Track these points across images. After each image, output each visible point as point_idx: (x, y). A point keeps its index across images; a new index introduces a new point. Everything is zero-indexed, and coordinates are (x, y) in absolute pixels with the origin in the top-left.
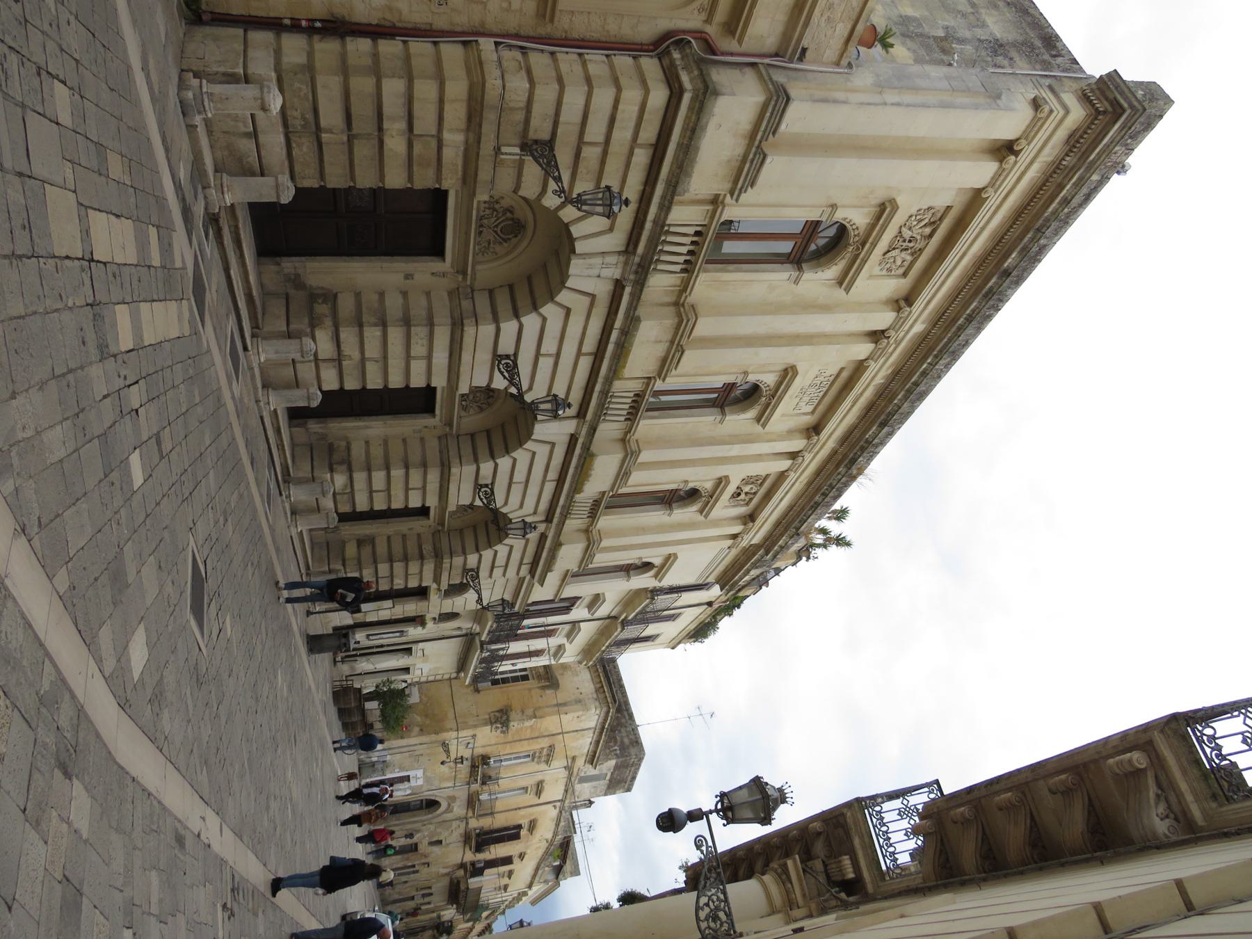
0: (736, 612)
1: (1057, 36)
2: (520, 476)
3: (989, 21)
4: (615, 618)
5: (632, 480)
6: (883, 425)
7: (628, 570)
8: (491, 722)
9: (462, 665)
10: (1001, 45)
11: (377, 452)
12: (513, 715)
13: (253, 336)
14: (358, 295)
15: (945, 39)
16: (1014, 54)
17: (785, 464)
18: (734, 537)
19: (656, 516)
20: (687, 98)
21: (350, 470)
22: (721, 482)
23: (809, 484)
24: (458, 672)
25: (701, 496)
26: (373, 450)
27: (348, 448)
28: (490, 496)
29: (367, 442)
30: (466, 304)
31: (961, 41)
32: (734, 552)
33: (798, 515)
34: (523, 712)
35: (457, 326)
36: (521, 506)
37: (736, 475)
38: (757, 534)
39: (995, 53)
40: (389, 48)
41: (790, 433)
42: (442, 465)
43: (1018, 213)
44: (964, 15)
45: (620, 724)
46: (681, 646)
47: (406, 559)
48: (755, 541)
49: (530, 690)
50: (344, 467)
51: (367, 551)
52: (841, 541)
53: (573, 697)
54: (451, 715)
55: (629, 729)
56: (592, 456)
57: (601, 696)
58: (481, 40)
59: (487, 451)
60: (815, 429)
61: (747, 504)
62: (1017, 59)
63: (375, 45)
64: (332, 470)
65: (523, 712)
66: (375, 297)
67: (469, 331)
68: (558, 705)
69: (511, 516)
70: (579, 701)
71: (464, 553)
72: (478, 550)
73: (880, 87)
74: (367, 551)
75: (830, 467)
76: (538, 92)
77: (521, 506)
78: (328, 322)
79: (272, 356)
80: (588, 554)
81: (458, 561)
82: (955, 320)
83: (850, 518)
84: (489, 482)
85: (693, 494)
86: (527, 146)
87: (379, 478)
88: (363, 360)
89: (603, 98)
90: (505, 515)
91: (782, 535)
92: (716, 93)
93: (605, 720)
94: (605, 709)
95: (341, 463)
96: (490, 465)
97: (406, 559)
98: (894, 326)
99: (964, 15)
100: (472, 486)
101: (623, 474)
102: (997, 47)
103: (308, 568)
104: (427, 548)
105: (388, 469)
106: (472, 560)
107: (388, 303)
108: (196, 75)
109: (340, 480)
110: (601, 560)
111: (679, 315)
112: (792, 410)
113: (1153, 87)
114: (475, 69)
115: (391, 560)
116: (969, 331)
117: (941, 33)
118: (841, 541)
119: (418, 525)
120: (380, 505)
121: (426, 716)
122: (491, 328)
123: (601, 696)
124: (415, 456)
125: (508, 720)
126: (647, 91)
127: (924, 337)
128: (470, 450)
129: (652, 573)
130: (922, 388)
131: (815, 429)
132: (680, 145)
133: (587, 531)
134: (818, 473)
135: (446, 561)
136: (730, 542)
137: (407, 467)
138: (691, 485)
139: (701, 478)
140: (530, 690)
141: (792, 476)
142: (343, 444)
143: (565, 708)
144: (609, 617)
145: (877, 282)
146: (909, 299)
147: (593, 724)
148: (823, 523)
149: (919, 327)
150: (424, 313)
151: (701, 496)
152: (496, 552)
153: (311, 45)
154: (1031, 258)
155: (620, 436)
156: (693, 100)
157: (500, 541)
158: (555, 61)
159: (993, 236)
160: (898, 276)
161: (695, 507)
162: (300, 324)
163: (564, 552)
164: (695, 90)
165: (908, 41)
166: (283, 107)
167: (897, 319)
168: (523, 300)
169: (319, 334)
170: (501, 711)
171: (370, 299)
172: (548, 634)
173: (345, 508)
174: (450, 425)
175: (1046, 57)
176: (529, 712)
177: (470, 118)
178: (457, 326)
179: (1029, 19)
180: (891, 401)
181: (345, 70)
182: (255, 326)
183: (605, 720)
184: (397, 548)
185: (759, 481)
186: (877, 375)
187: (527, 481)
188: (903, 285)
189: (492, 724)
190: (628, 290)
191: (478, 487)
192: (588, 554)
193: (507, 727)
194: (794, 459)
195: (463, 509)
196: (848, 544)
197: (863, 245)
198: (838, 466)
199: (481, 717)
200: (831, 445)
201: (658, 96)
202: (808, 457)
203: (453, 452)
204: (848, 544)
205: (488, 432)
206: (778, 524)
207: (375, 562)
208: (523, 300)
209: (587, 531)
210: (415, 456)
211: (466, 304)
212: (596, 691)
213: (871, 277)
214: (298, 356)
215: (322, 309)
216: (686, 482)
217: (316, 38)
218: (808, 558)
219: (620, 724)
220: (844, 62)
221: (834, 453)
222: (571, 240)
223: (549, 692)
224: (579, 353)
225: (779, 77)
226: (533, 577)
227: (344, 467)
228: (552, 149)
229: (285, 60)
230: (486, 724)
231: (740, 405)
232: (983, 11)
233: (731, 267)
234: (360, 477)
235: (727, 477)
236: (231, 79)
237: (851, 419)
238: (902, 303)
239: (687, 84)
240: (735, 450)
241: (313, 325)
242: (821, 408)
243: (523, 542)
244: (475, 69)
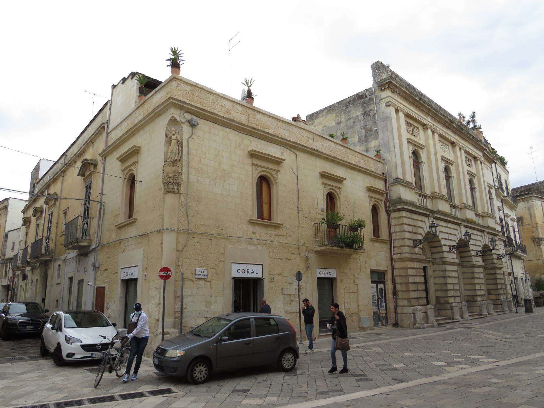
0: (385, 64)
1: (358, 94)
2: (446, 236)
3: (355, 115)
4: (502, 200)
5: (410, 180)
6: (453, 122)
7: (491, 199)
8: (539, 245)
9: (519, 258)
10: (365, 113)
11: (469, 287)
12: (536, 236)
13: (453, 319)
14: (436, 291)
15: (366, 130)
16: (368, 109)
17: (462, 151)
18: (481, 163)
19: (424, 168)
20: (405, 207)
21: (476, 295)
22: (409, 142)
23: (466, 141)
24: (521, 259)
25: (416, 150)
26: (468, 288)
27: (468, 296)
28: (419, 241)
29: (465, 290)
30: (438, 260)
31: (366, 125)
32: (486, 162)
33: (475, 142)
34: (534, 232)
35: (445, 263)
36: (455, 235)
37: (405, 135)
38: (479, 154)
39: (369, 115)
40: (398, 280)
41: (454, 152)
42: (472, 267)
43: (407, 100)
44: (354, 122)
45: (537, 189)
46: (507, 169)
47: (496, 279)
48: (481, 154)
49: (523, 229)
50: (475, 297)
51: (493, 292)
52: (473, 116)
53: (527, 211)
54: (536, 262)
55: (540, 185)
56: (467, 219)
57: (526, 199)
58: (393, 258)
59: (440, 248)
60: (453, 144)
61: (418, 128)
62: (370, 108)
63: (398, 283)
64: (476, 301)
65: (534, 232)
66: (437, 286)
67: (447, 260)
68: (531, 217)
69: (426, 232)
70: (529, 209)
71: (493, 259)
72: (441, 246)
73: (389, 152)
74: (493, 292)
75: (462, 135)
76: (407, 244)
77: (455, 235)
78: (447, 299)
79: (459, 315)
80: (442, 198)
81: (474, 259)
82: (429, 110)
83: (463, 113)
84: (448, 247)
85: (415, 154)
86: (415, 246)
87: (478, 287)
88: (454, 290)
89: (406, 228)
90: (426, 234)
91: (481, 146)
92: (400, 198)
93: (538, 197)
94: (533, 198)
95: (473, 298)
96: (444, 247)
97: (445, 277)
98: (402, 112)
99: (354, 122)
100: (450, 254)
101: (407, 185)
102: (366, 114)
103: (500, 311)
104: (491, 272)
105: (475, 284)
106: (495, 257)
107: (438, 282)
108: (415, 324)
109: (479, 299)
110: (444, 192)
111: (436, 198)
112: (450, 156)
113: (373, 66)
114: (402, 260)
115: (497, 284)
116: (433, 105)
117: (364, 131)
118: (473, 116)
119: (430, 272)
120: (423, 287)
121: (536, 272)
122: (445, 253)
123: (526, 199)
124: (470, 275)
125: (538, 238)
126: (403, 217)
127: (432, 117)
128: (467, 258)
129: (473, 178)
130: (438, 109)
131: (453, 144)
132: (412, 207)
133: (483, 217)
134: (463, 139)
135: (497, 265)
136: (483, 164)
137: (474, 278)
138: (411, 155)
139: (408, 150)
140: (523, 229)
141: (466, 149)
142: (466, 297)
143: (532, 214)
144: (502, 202)
145: (421, 138)
146: (424, 125)
147: (539, 203)
148: (465, 123)
149: (429, 119)
150: (441, 273)
151: (416, 150)
152: (442, 238)
153: (400, 299)
154: (410, 87)
155: (430, 200)
156: (405, 205)
157: (438, 237)
158: (396, 239)
159: (410, 105)
160: (419, 131)
161: (451, 167)
162: (448, 307)
163: (490, 225)
164: (403, 205)
165: (369, 140)
166: (420, 305)
167: (393, 106)
168: (437, 244)
169: (450, 302)
170: (534, 241)
171: (437, 287)
172: (507, 225)
173: (424, 301)
174: (429, 261)
175: (367, 99)
176: (534, 229)
177: (412, 261)
178: (445, 263)
179: (352, 102)
180: (446, 122)
181: (408, 291)
182: (450, 319)
183: (538, 197)
184: (492, 282)
185: (408, 124)
186: (441, 129)
187: (474, 240)
188: (420, 127)
189: (540, 245)
190: (436, 215)
191: (450, 252)
192: (469, 208)
193: (541, 239)
194: (398, 111)
195: (424, 253)
196: (474, 113)
197: (416, 145)
198: (462, 133)
199: (537, 249)
200: (457, 137)
201: (404, 213)
202: (461, 144)
203: (468, 264)
204: (474, 113)
205: (431, 247)
206: (477, 148)
207: (497, 289)
208: (437, 244)
209: (483, 217)
210: (470, 275)
211: (438, 260)
212: (524, 201)
213: (420, 139)
214: (458, 308)
215: (442, 300)
216: (410, 157)
217: (397, 297)
218: (480, 128)
219: (537, 189)
220: (383, 162)
221: (459, 135)
222: (428, 232)
223: (524, 221)
224: (447, 227)
225: (392, 181)
226: (498, 235)
227: (475, 297)
228: (416, 240)
229: (406, 305)
230: (540, 248)
231: (418, 155)
232: (351, 116)
233: (422, 184)
234: (478, 293)
235: (407, 139)
236: (415, 318)
237: (450, 132)
238: (425, 127)
239: (402, 207)
240: (461, 171)
241: (448, 303)
242: (447, 143)
243: (438, 227)
244: (402, 260)
